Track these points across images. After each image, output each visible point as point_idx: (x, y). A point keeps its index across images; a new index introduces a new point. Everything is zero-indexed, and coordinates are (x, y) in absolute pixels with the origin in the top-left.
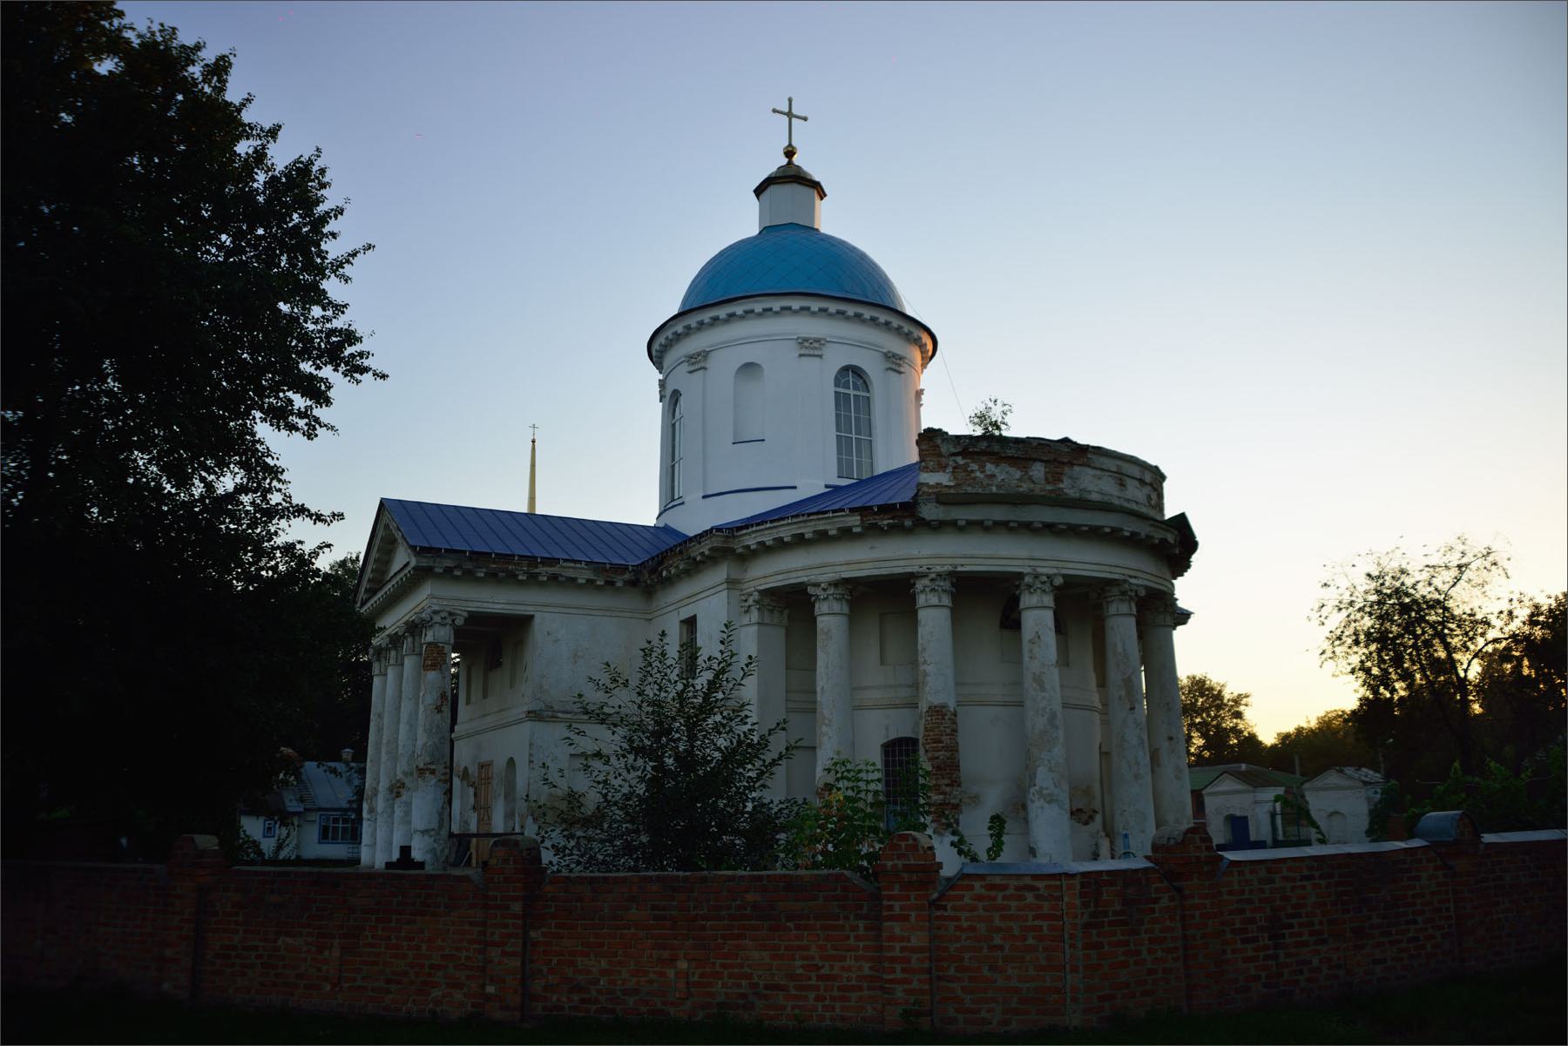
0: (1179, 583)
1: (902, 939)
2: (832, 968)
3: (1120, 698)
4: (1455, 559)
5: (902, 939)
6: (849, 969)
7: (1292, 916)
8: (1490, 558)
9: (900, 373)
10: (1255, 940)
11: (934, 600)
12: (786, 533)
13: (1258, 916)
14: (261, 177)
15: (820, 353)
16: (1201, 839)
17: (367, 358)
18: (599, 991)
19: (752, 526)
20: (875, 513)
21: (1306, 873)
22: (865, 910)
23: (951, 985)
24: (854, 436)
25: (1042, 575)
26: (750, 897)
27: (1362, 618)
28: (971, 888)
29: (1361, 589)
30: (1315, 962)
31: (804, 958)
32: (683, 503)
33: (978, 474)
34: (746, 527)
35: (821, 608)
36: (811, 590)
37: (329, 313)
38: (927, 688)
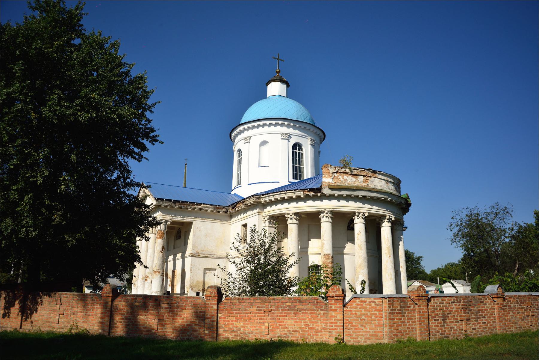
0: (405, 216)
1: (335, 317)
2: (313, 325)
3: (386, 253)
4: (495, 210)
5: (335, 317)
6: (318, 326)
7: (449, 314)
8: (506, 211)
10: (438, 320)
11: (326, 219)
12: (279, 197)
13: (439, 313)
14: (128, 80)
16: (422, 289)
17: (158, 137)
18: (241, 333)
19: (267, 194)
20: (308, 191)
21: (453, 301)
22: (323, 308)
23: (349, 330)
24: (298, 166)
25: (361, 212)
26: (288, 304)
27: (464, 229)
28: (356, 302)
29: (464, 220)
30: (455, 328)
31: (305, 322)
32: (241, 186)
33: (342, 179)
34: (266, 194)
35: (289, 221)
36: (286, 216)
37: (147, 122)
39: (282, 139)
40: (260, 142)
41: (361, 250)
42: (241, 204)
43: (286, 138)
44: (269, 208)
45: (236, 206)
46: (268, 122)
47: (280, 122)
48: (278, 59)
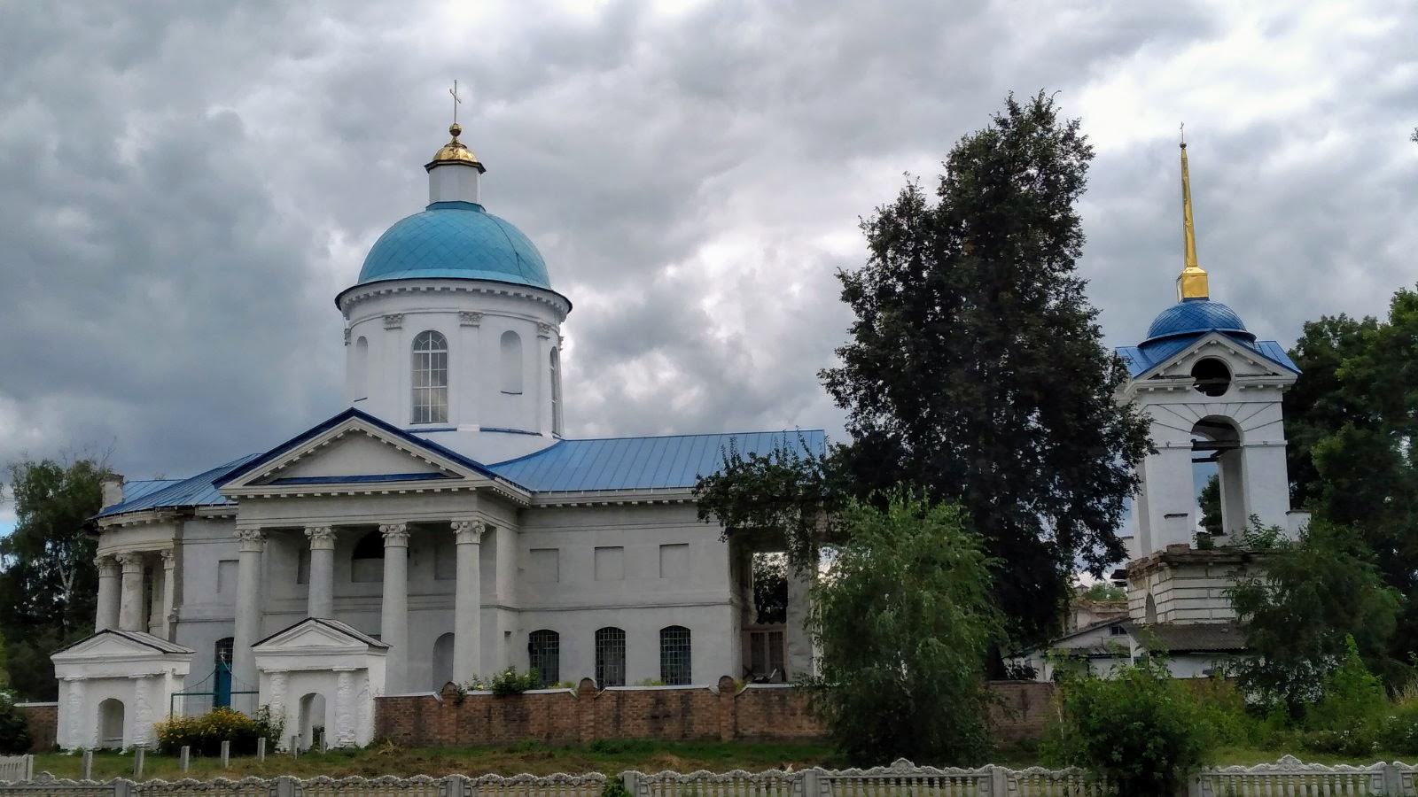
9: (547, 338)
15: (477, 324)
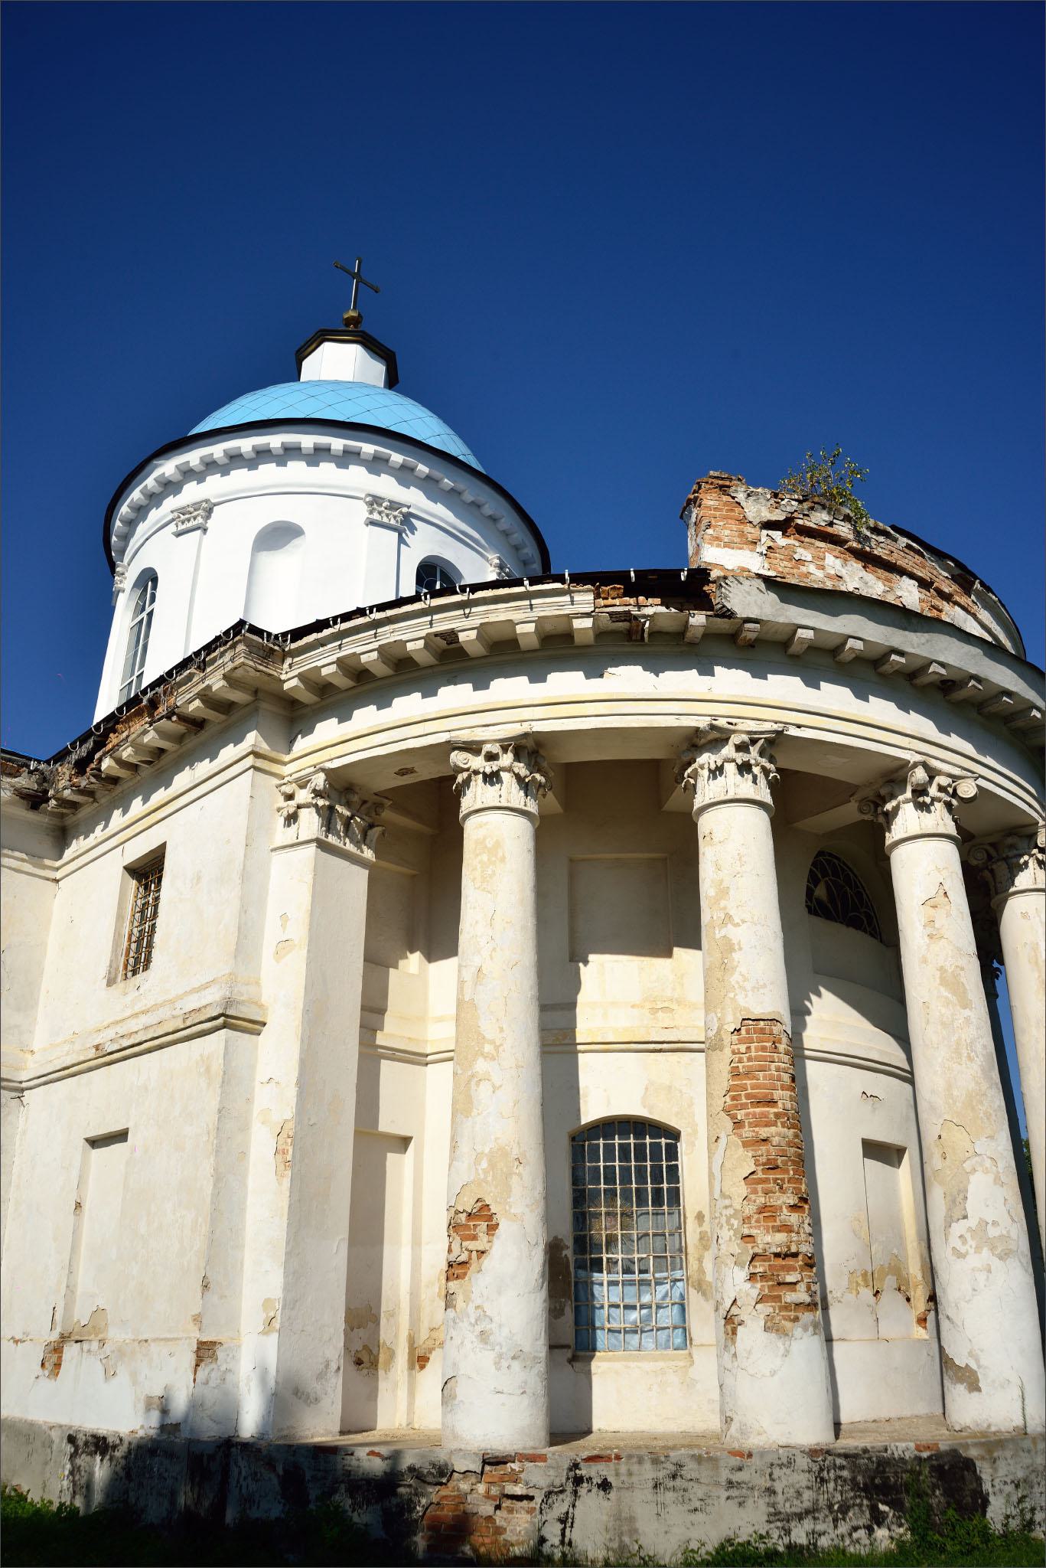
33: (812, 568)
38: (735, 978)
39: (372, 523)
40: (260, 528)
41: (965, 1004)
42: (138, 726)
43: (393, 522)
44: (328, 730)
45: (100, 744)
46: (308, 441)
47: (368, 449)
48: (357, 276)
